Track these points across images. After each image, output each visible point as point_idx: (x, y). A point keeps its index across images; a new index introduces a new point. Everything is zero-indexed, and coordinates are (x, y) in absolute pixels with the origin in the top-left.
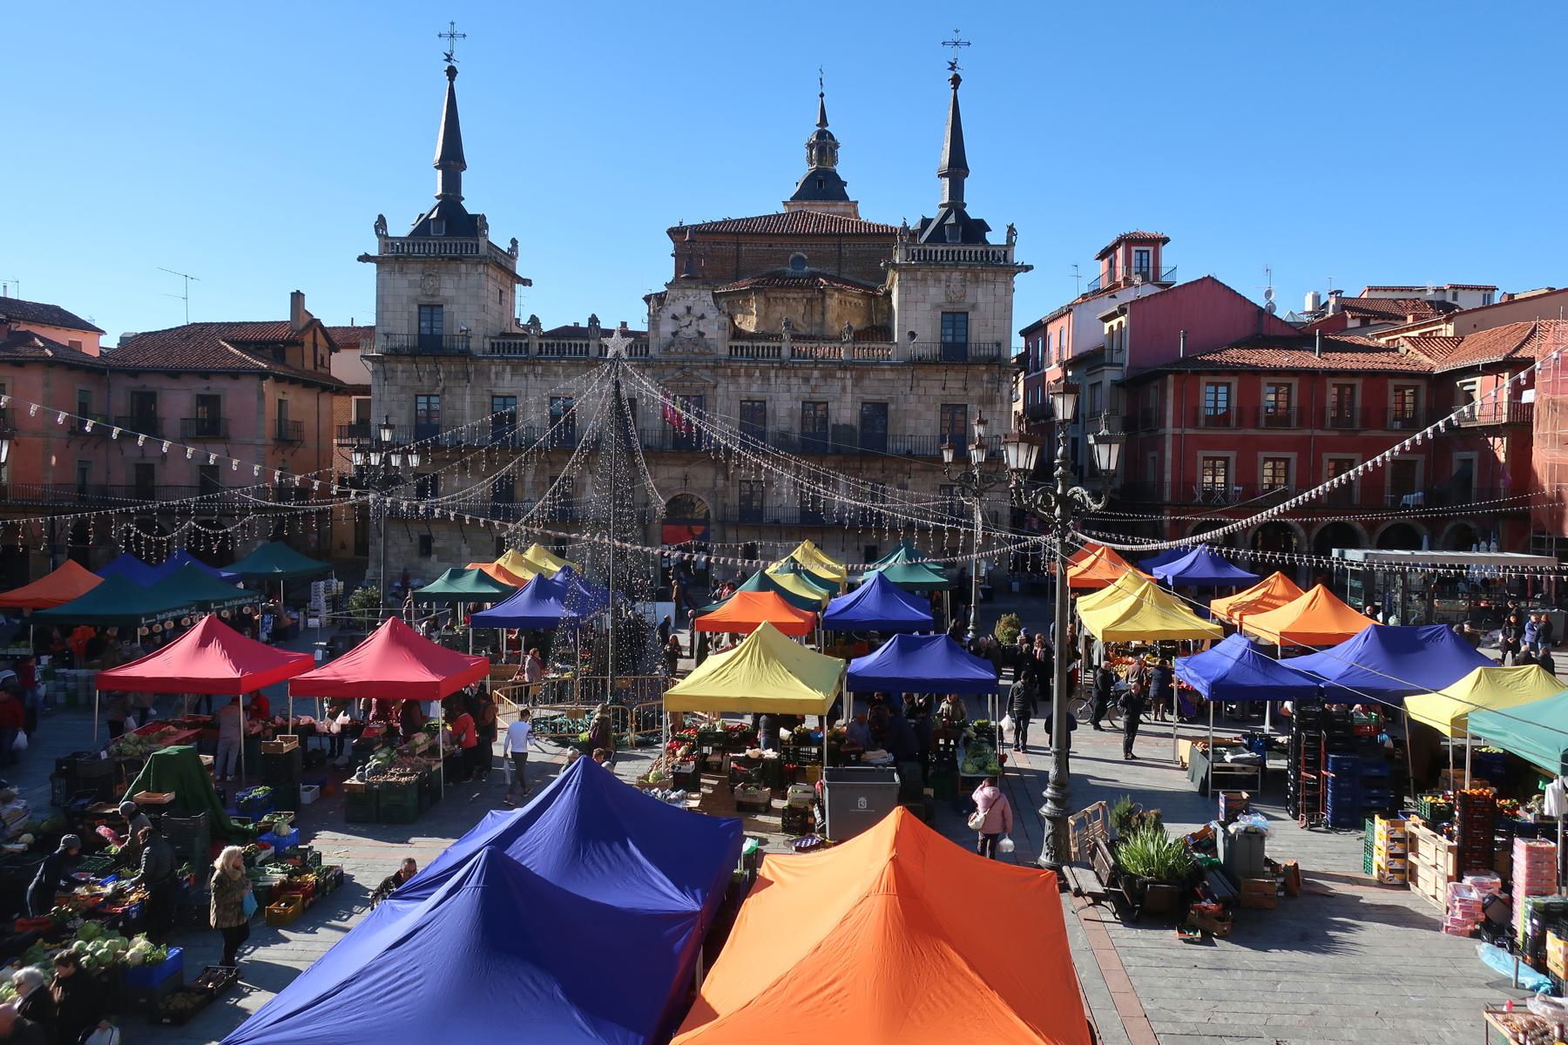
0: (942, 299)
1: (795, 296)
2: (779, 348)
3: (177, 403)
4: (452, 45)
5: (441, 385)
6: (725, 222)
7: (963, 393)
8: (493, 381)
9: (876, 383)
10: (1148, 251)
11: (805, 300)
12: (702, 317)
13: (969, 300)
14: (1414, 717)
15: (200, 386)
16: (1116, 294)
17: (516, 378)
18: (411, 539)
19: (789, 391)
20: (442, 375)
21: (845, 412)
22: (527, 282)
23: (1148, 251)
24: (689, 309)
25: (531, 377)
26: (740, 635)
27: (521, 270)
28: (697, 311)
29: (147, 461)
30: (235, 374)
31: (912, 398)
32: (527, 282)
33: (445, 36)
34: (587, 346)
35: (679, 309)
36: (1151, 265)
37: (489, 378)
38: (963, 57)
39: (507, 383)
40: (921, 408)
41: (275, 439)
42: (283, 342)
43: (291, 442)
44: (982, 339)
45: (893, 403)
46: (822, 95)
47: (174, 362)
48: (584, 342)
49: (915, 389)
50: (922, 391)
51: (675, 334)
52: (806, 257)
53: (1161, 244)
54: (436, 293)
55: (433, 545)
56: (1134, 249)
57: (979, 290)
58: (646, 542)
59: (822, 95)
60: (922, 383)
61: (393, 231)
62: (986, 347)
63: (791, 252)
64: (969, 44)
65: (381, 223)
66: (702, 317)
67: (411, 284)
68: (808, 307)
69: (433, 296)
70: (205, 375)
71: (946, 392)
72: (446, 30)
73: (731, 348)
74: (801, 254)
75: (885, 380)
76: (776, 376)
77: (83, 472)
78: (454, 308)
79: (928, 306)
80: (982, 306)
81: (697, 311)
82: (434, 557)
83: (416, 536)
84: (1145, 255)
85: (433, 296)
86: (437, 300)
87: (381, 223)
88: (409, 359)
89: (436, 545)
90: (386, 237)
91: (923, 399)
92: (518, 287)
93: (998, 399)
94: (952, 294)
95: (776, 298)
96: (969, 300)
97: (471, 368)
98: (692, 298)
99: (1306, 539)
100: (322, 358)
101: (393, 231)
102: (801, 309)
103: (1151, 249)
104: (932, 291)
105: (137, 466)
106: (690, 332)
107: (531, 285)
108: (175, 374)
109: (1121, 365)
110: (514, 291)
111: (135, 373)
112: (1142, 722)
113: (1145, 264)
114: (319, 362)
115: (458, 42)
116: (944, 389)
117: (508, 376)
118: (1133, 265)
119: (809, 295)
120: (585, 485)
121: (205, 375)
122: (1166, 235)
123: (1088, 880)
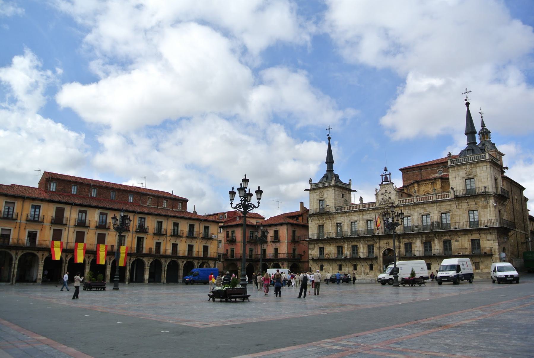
0: (464, 175)
1: (427, 182)
3: (271, 234)
4: (467, 95)
5: (324, 222)
6: (12, 186)
9: (445, 206)
11: (431, 183)
12: (390, 193)
15: (274, 228)
17: (342, 218)
18: (318, 266)
20: (324, 219)
25: (346, 217)
27: (352, 188)
31: (457, 210)
33: (469, 92)
35: (383, 191)
38: (470, 96)
40: (461, 213)
41: (291, 241)
42: (297, 216)
43: (297, 242)
47: (269, 224)
49: (458, 206)
50: (460, 207)
51: (383, 199)
55: (323, 267)
60: (460, 204)
61: (313, 182)
62: (482, 189)
63: (437, 169)
65: (310, 181)
67: (317, 195)
68: (432, 186)
69: (322, 197)
72: (464, 91)
75: (448, 205)
79: (460, 178)
80: (479, 175)
82: (324, 271)
83: (319, 265)
85: (322, 197)
87: (310, 181)
89: (324, 267)
91: (461, 209)
95: (421, 184)
98: (387, 187)
101: (313, 182)
106: (386, 198)
115: (469, 94)
119: (432, 181)
120: (360, 247)
123: (259, 243)
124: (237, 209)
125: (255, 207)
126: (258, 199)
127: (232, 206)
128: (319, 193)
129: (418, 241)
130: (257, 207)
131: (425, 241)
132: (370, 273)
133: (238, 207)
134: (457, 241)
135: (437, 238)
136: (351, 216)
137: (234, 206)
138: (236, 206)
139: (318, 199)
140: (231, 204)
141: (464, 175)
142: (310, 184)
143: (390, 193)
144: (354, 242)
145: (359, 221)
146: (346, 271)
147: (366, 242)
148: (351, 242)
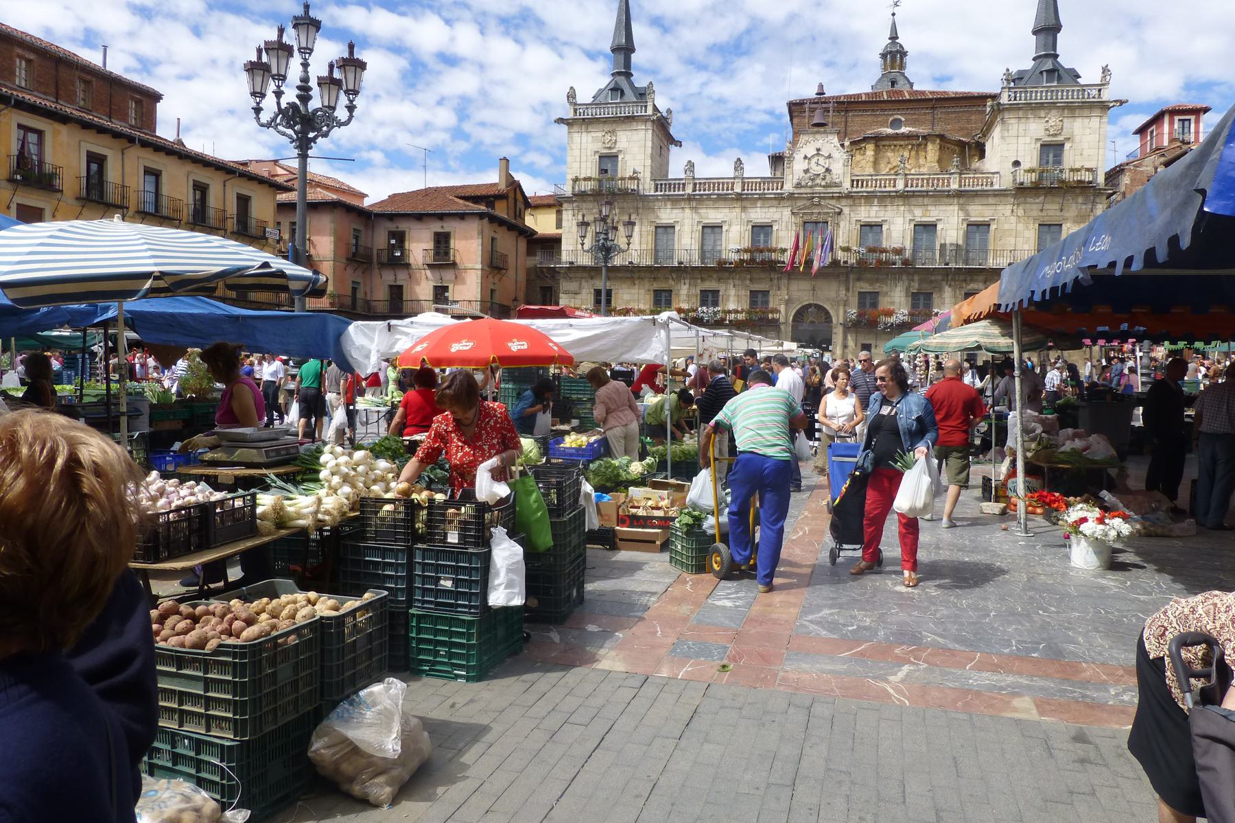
1: (902, 143)
7: (1058, 213)
10: (1189, 120)
12: (829, 157)
15: (437, 227)
23: (1189, 120)
24: (818, 150)
26: (1033, 308)
29: (399, 283)
30: (462, 216)
39: (667, 215)
42: (491, 196)
46: (893, 14)
51: (806, 171)
53: (1202, 114)
56: (1176, 118)
59: (893, 14)
61: (579, 100)
65: (571, 95)
70: (441, 217)
71: (1044, 213)
73: (853, 181)
74: (899, 117)
77: (354, 290)
78: (627, 157)
81: (824, 152)
84: (1186, 123)
87: (571, 95)
88: (591, 198)
90: (575, 104)
92: (673, 149)
95: (884, 146)
97: (640, 205)
101: (579, 100)
103: (1193, 118)
105: (391, 286)
107: (681, 146)
108: (420, 217)
111: (391, 217)
112: (224, 752)
116: (1042, 210)
121: (441, 217)
124: (276, 128)
125: (340, 124)
126: (254, 94)
127: (258, 119)
128: (600, 134)
129: (898, 289)
130: (347, 123)
131: (915, 291)
133: (278, 121)
135: (950, 286)
137: (265, 117)
138: (274, 119)
139: (596, 152)
140: (258, 110)
142: (571, 103)
143: (829, 157)
144: (711, 281)
147: (748, 282)
148: (699, 281)
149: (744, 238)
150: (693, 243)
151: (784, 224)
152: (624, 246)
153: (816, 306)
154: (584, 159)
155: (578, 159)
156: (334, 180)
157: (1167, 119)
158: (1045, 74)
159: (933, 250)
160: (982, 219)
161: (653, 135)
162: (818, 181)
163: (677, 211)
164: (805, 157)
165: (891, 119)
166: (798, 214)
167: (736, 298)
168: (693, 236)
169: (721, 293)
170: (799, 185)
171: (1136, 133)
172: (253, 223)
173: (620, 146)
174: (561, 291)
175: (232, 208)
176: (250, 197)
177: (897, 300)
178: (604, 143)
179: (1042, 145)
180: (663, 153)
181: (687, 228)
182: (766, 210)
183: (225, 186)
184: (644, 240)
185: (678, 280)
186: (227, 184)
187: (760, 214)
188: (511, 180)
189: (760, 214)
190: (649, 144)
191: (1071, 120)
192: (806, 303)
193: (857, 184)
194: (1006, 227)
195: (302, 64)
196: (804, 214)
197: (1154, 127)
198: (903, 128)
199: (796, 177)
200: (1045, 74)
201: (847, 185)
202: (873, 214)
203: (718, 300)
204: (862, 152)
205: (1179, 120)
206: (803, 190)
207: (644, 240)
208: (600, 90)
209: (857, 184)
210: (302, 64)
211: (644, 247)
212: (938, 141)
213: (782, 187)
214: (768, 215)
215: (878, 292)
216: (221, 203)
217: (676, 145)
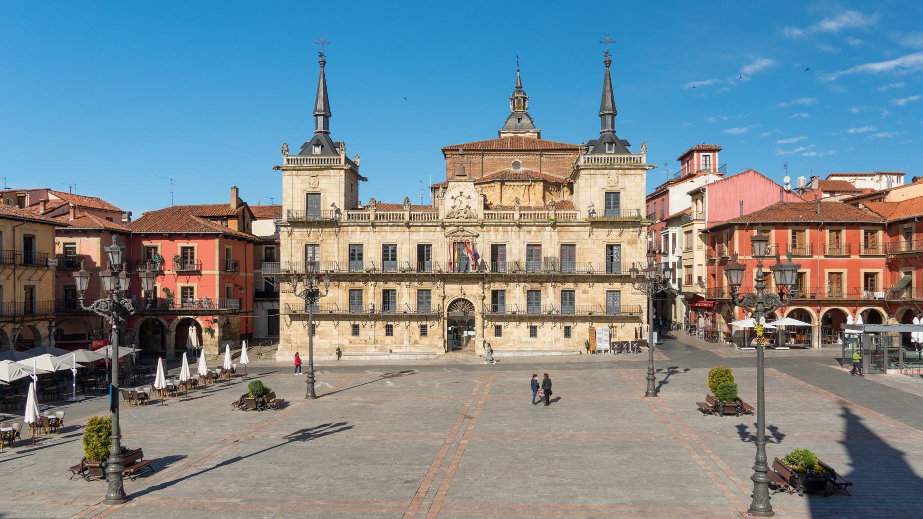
2: (513, 214)
8: (350, 236)
10: (709, 156)
12: (469, 197)
13: (620, 185)
14: (264, 386)
16: (694, 180)
17: (363, 234)
19: (519, 239)
21: (551, 249)
22: (365, 179)
24: (461, 193)
27: (361, 172)
28: (456, 194)
32: (365, 179)
34: (403, 214)
36: (712, 163)
37: (348, 234)
40: (594, 246)
44: (629, 207)
45: (509, 244)
48: (402, 213)
51: (453, 207)
52: (521, 162)
54: (316, 186)
56: (701, 154)
57: (626, 179)
58: (103, 317)
62: (632, 211)
63: (513, 159)
64: (615, 42)
66: (469, 197)
68: (526, 190)
73: (485, 214)
76: (512, 231)
78: (328, 195)
79: (597, 189)
81: (456, 194)
84: (708, 158)
86: (317, 190)
91: (595, 241)
92: (360, 182)
93: (639, 241)
94: (611, 182)
96: (620, 185)
98: (463, 187)
99: (817, 319)
100: (248, 224)
102: (522, 192)
103: (711, 154)
104: (600, 180)
107: (367, 180)
109: (704, 220)
110: (358, 184)
113: (708, 163)
114: (246, 227)
117: (358, 233)
118: (701, 163)
122: (718, 145)
132: (421, 342)
134: (585, 292)
136: (384, 233)
141: (605, 185)
145: (402, 244)
146: (371, 337)
149: (412, 253)
150: (376, 256)
151: (440, 243)
152: (324, 293)
153: (463, 300)
154: (295, 195)
155: (291, 196)
156: (97, 199)
157: (695, 154)
158: (607, 144)
159: (540, 259)
160: (570, 241)
161: (345, 179)
162: (462, 214)
163: (364, 234)
164: (453, 198)
165: (513, 162)
166: (449, 236)
167: (408, 295)
168: (376, 252)
169: (397, 292)
170: (448, 217)
171: (679, 160)
172: (37, 256)
173: (321, 186)
174: (281, 291)
175: (20, 247)
176: (34, 236)
177: (518, 296)
178: (310, 184)
179: (606, 193)
180: (353, 188)
181: (372, 246)
182: (427, 233)
183: (14, 230)
184: (341, 254)
185: (366, 281)
186: (16, 228)
187: (422, 236)
188: (240, 202)
189: (422, 236)
190: (343, 186)
191: (624, 177)
192: (457, 298)
193: (488, 217)
194: (586, 246)
195: (139, 453)
196: (453, 236)
197: (689, 158)
198: (521, 168)
199: (446, 212)
200: (607, 144)
201: (481, 216)
202: (499, 237)
203: (395, 296)
204: (492, 189)
205: (703, 156)
206: (452, 220)
207: (341, 254)
208: (306, 143)
209: (488, 217)
210: (139, 453)
211: (341, 259)
212: (542, 183)
213: (438, 218)
214: (429, 237)
215: (505, 290)
216: (11, 243)
217: (363, 181)
